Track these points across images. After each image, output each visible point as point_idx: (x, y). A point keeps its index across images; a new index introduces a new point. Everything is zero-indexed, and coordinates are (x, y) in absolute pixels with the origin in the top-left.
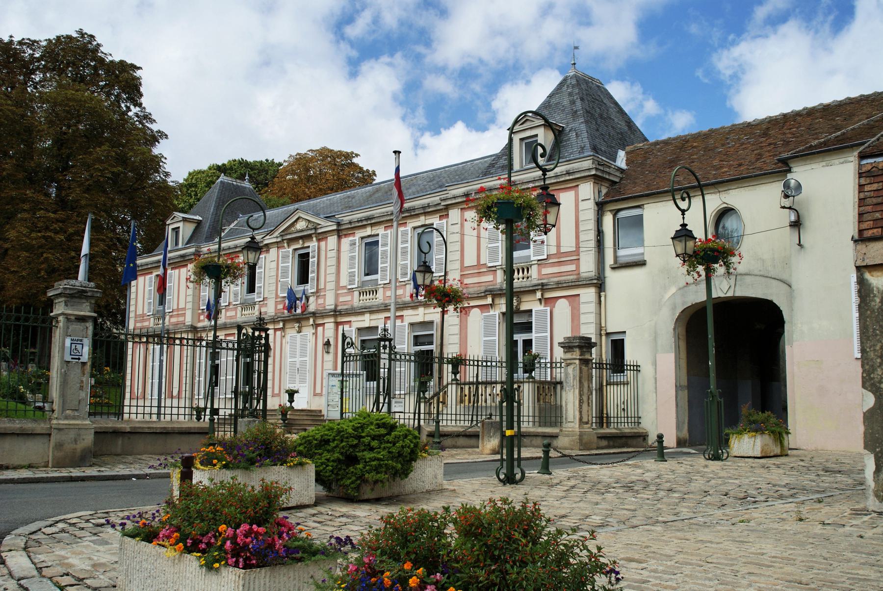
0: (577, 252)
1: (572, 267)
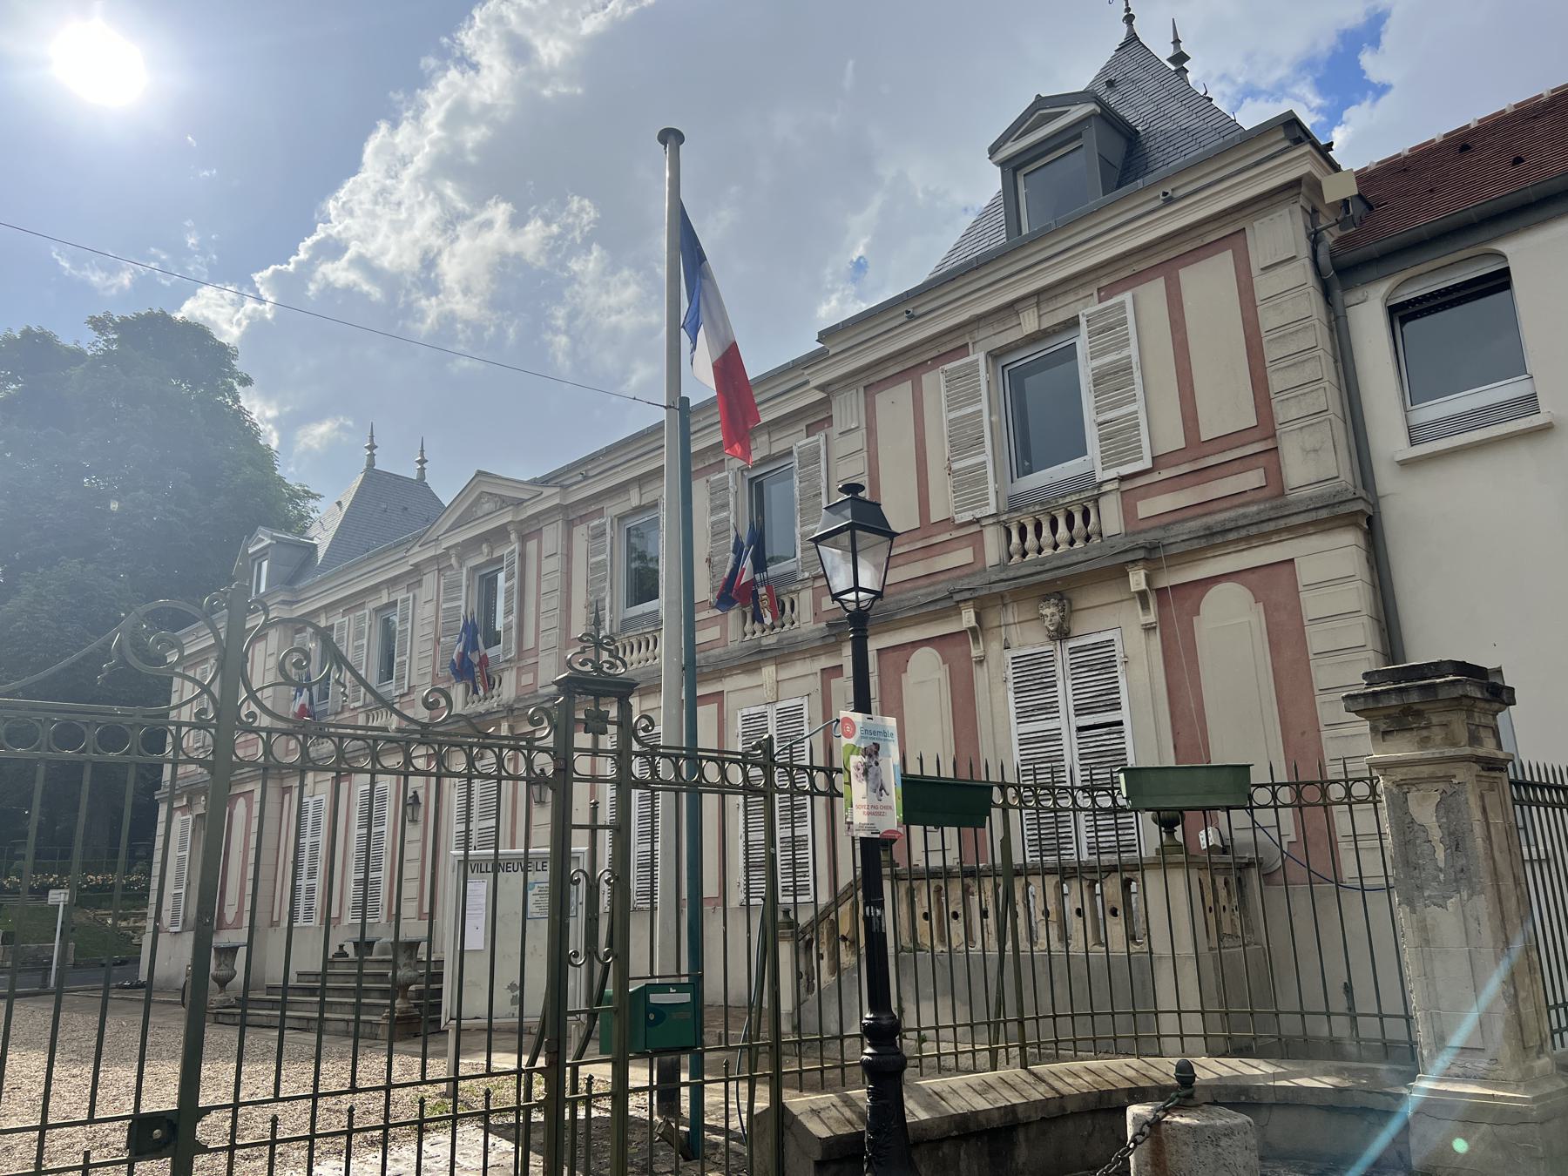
0: (1266, 427)
1: (1254, 479)
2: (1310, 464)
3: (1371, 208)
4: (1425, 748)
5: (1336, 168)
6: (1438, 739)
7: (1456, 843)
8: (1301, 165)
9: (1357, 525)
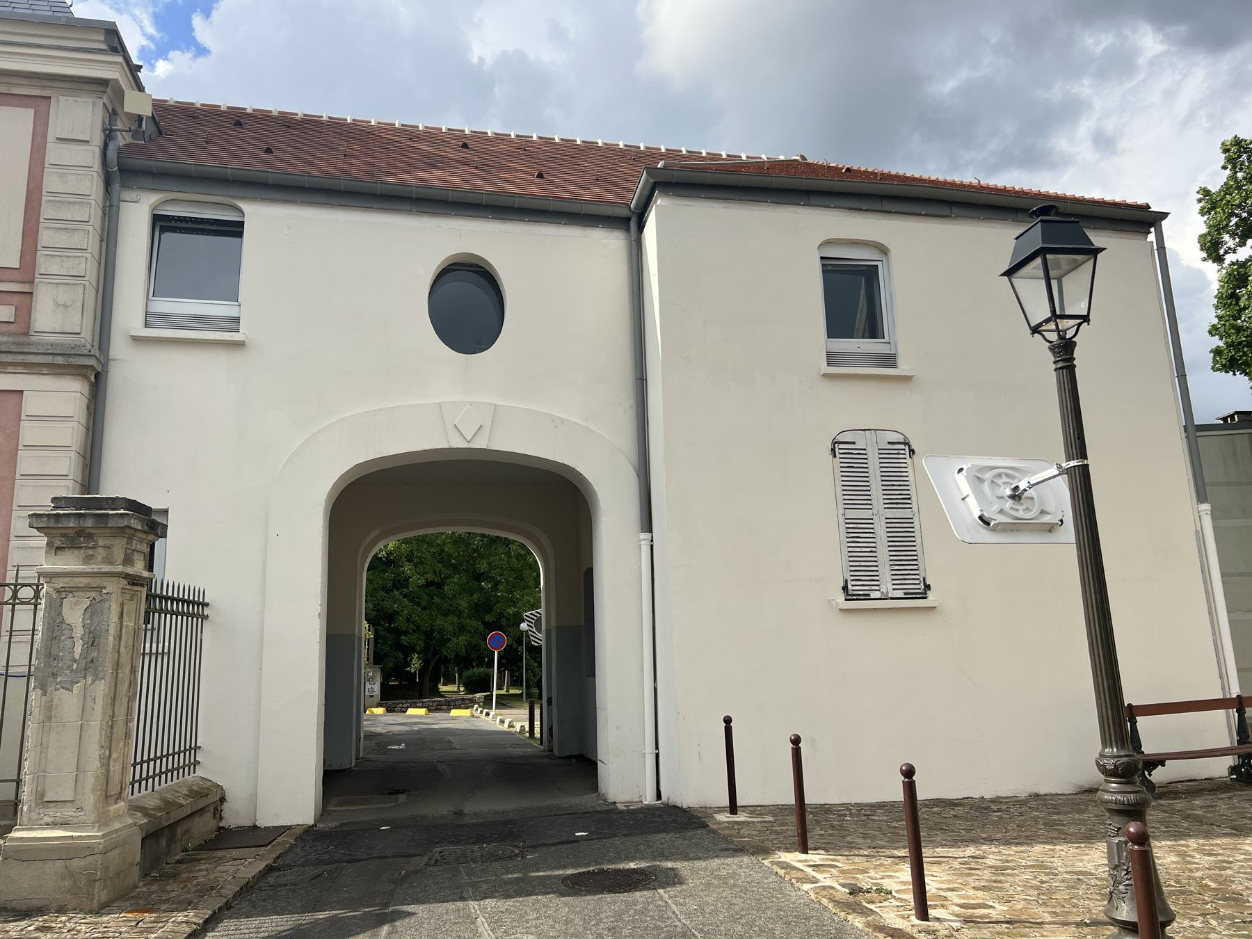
2: (57, 315)
3: (160, 133)
4: (88, 564)
5: (140, 88)
6: (99, 558)
7: (93, 640)
8: (110, 70)
9: (86, 377)
